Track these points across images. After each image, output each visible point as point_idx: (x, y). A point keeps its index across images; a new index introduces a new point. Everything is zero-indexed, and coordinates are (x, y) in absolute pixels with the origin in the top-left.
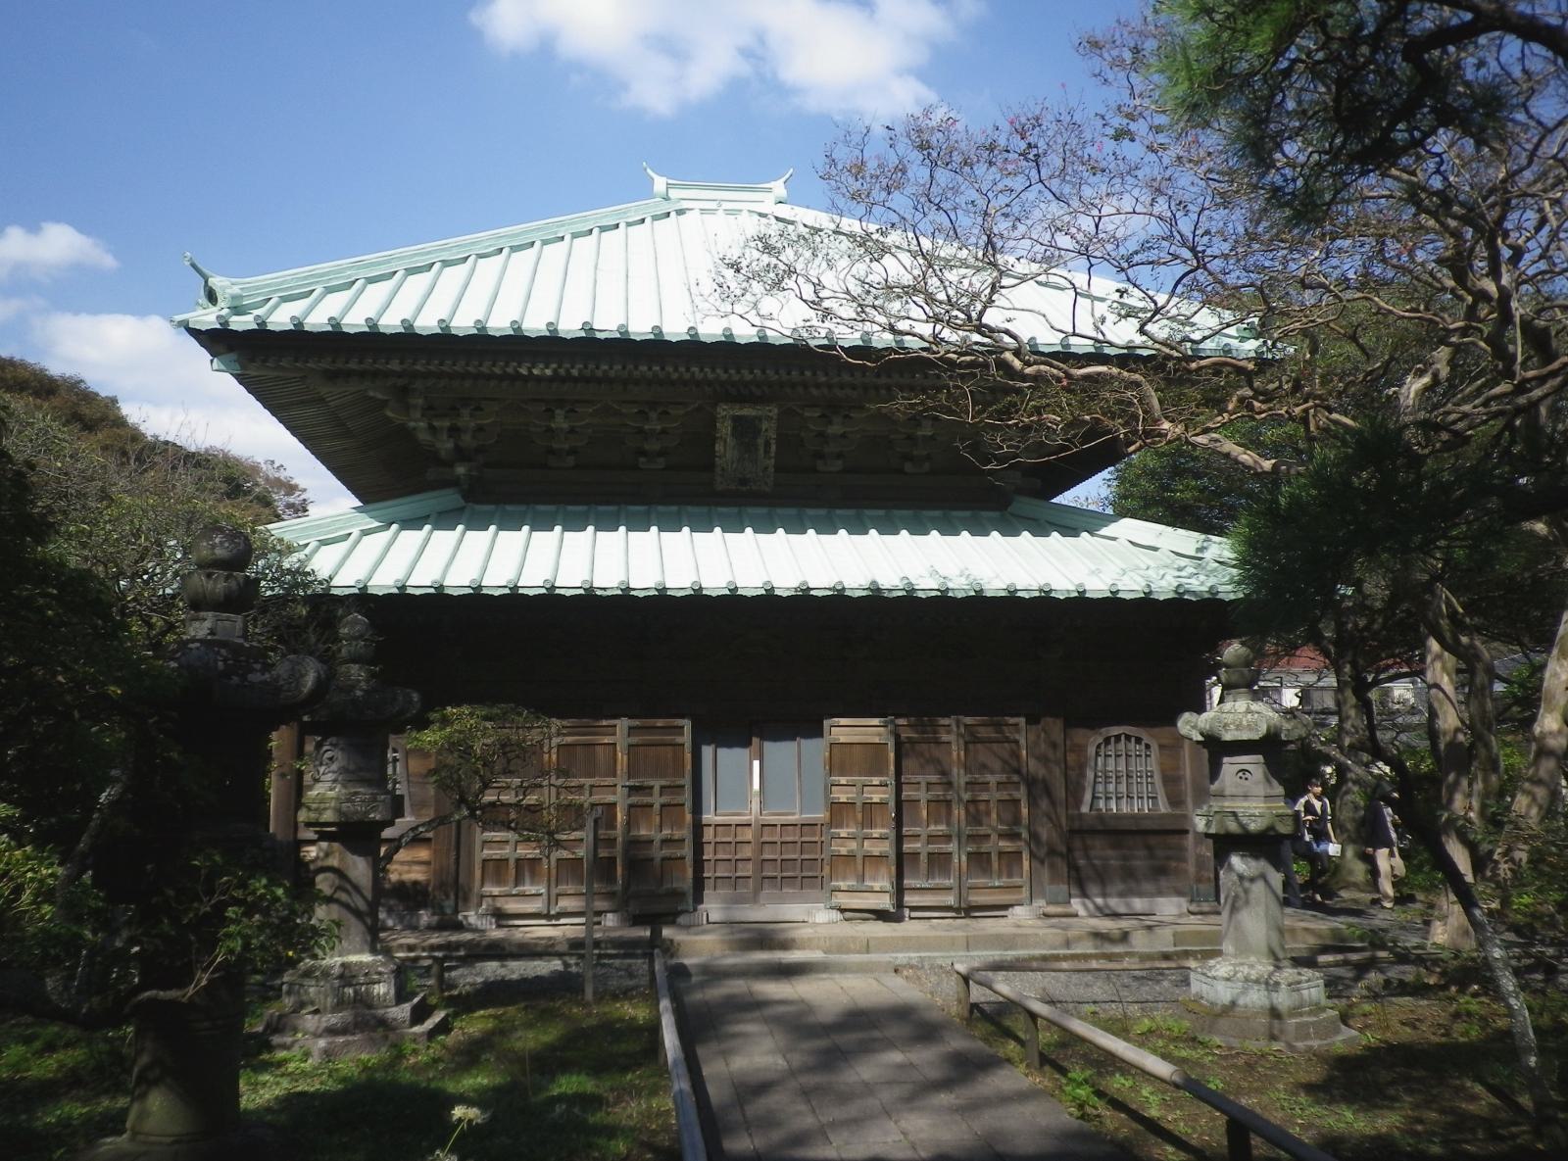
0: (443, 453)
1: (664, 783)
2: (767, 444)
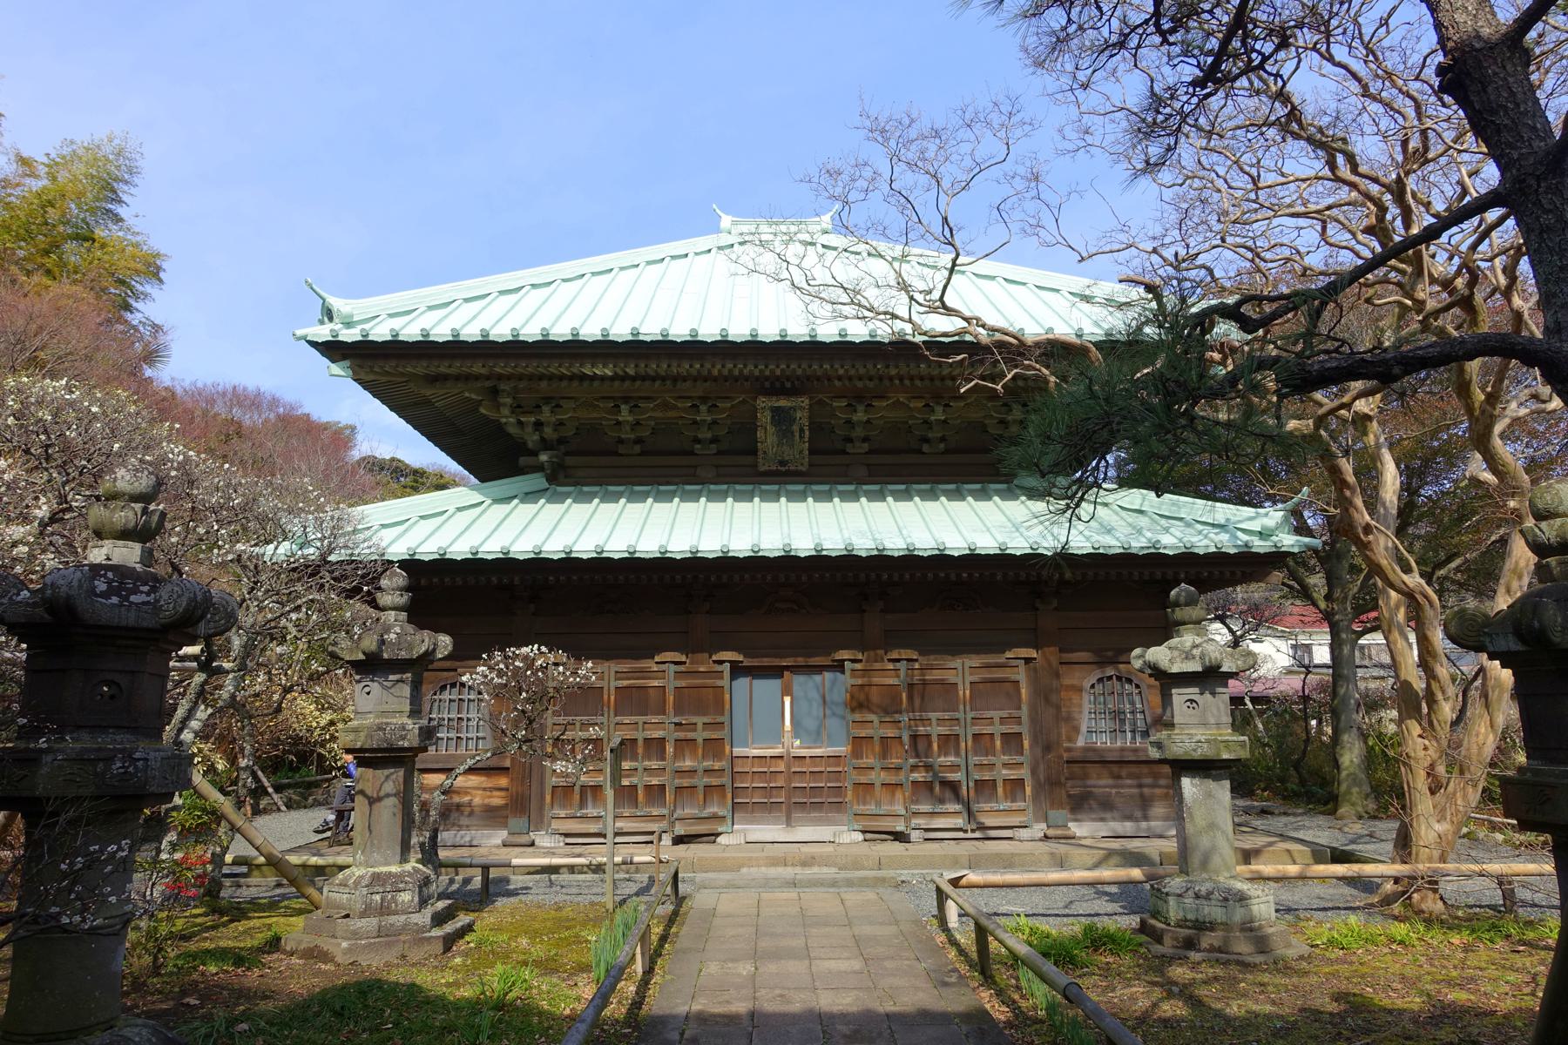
0: (530, 445)
1: (706, 720)
2: (802, 431)
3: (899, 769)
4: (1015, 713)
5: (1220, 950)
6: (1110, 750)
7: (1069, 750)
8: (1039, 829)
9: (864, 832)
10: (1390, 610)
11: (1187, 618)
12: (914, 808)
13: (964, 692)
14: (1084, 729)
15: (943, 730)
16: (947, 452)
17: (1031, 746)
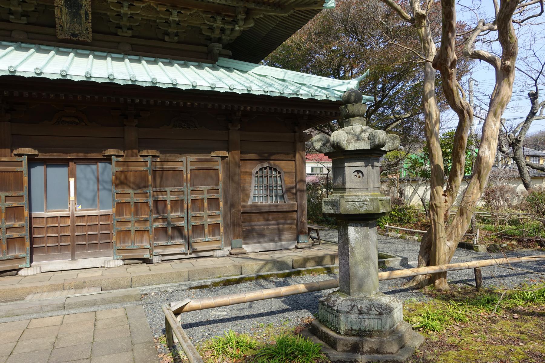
1: (8, 194)
2: (86, 14)
3: (146, 221)
4: (215, 187)
5: (378, 352)
6: (265, 206)
7: (244, 207)
8: (227, 250)
9: (123, 260)
10: (432, 125)
11: (356, 112)
12: (156, 243)
13: (187, 175)
14: (252, 195)
15: (174, 197)
16: (179, 42)
17: (224, 205)
